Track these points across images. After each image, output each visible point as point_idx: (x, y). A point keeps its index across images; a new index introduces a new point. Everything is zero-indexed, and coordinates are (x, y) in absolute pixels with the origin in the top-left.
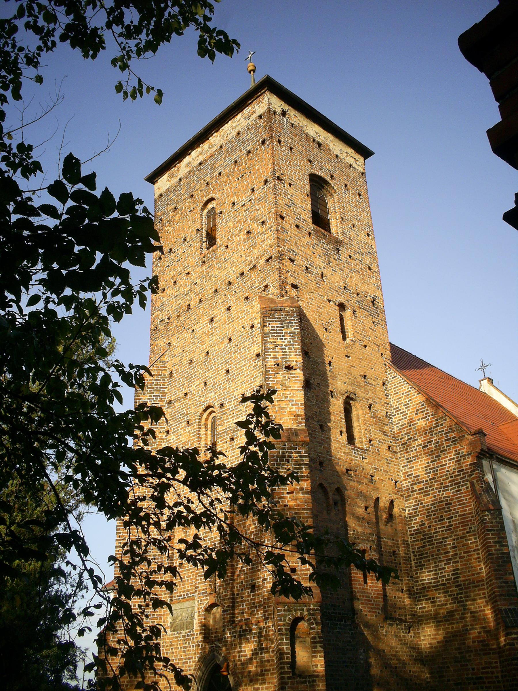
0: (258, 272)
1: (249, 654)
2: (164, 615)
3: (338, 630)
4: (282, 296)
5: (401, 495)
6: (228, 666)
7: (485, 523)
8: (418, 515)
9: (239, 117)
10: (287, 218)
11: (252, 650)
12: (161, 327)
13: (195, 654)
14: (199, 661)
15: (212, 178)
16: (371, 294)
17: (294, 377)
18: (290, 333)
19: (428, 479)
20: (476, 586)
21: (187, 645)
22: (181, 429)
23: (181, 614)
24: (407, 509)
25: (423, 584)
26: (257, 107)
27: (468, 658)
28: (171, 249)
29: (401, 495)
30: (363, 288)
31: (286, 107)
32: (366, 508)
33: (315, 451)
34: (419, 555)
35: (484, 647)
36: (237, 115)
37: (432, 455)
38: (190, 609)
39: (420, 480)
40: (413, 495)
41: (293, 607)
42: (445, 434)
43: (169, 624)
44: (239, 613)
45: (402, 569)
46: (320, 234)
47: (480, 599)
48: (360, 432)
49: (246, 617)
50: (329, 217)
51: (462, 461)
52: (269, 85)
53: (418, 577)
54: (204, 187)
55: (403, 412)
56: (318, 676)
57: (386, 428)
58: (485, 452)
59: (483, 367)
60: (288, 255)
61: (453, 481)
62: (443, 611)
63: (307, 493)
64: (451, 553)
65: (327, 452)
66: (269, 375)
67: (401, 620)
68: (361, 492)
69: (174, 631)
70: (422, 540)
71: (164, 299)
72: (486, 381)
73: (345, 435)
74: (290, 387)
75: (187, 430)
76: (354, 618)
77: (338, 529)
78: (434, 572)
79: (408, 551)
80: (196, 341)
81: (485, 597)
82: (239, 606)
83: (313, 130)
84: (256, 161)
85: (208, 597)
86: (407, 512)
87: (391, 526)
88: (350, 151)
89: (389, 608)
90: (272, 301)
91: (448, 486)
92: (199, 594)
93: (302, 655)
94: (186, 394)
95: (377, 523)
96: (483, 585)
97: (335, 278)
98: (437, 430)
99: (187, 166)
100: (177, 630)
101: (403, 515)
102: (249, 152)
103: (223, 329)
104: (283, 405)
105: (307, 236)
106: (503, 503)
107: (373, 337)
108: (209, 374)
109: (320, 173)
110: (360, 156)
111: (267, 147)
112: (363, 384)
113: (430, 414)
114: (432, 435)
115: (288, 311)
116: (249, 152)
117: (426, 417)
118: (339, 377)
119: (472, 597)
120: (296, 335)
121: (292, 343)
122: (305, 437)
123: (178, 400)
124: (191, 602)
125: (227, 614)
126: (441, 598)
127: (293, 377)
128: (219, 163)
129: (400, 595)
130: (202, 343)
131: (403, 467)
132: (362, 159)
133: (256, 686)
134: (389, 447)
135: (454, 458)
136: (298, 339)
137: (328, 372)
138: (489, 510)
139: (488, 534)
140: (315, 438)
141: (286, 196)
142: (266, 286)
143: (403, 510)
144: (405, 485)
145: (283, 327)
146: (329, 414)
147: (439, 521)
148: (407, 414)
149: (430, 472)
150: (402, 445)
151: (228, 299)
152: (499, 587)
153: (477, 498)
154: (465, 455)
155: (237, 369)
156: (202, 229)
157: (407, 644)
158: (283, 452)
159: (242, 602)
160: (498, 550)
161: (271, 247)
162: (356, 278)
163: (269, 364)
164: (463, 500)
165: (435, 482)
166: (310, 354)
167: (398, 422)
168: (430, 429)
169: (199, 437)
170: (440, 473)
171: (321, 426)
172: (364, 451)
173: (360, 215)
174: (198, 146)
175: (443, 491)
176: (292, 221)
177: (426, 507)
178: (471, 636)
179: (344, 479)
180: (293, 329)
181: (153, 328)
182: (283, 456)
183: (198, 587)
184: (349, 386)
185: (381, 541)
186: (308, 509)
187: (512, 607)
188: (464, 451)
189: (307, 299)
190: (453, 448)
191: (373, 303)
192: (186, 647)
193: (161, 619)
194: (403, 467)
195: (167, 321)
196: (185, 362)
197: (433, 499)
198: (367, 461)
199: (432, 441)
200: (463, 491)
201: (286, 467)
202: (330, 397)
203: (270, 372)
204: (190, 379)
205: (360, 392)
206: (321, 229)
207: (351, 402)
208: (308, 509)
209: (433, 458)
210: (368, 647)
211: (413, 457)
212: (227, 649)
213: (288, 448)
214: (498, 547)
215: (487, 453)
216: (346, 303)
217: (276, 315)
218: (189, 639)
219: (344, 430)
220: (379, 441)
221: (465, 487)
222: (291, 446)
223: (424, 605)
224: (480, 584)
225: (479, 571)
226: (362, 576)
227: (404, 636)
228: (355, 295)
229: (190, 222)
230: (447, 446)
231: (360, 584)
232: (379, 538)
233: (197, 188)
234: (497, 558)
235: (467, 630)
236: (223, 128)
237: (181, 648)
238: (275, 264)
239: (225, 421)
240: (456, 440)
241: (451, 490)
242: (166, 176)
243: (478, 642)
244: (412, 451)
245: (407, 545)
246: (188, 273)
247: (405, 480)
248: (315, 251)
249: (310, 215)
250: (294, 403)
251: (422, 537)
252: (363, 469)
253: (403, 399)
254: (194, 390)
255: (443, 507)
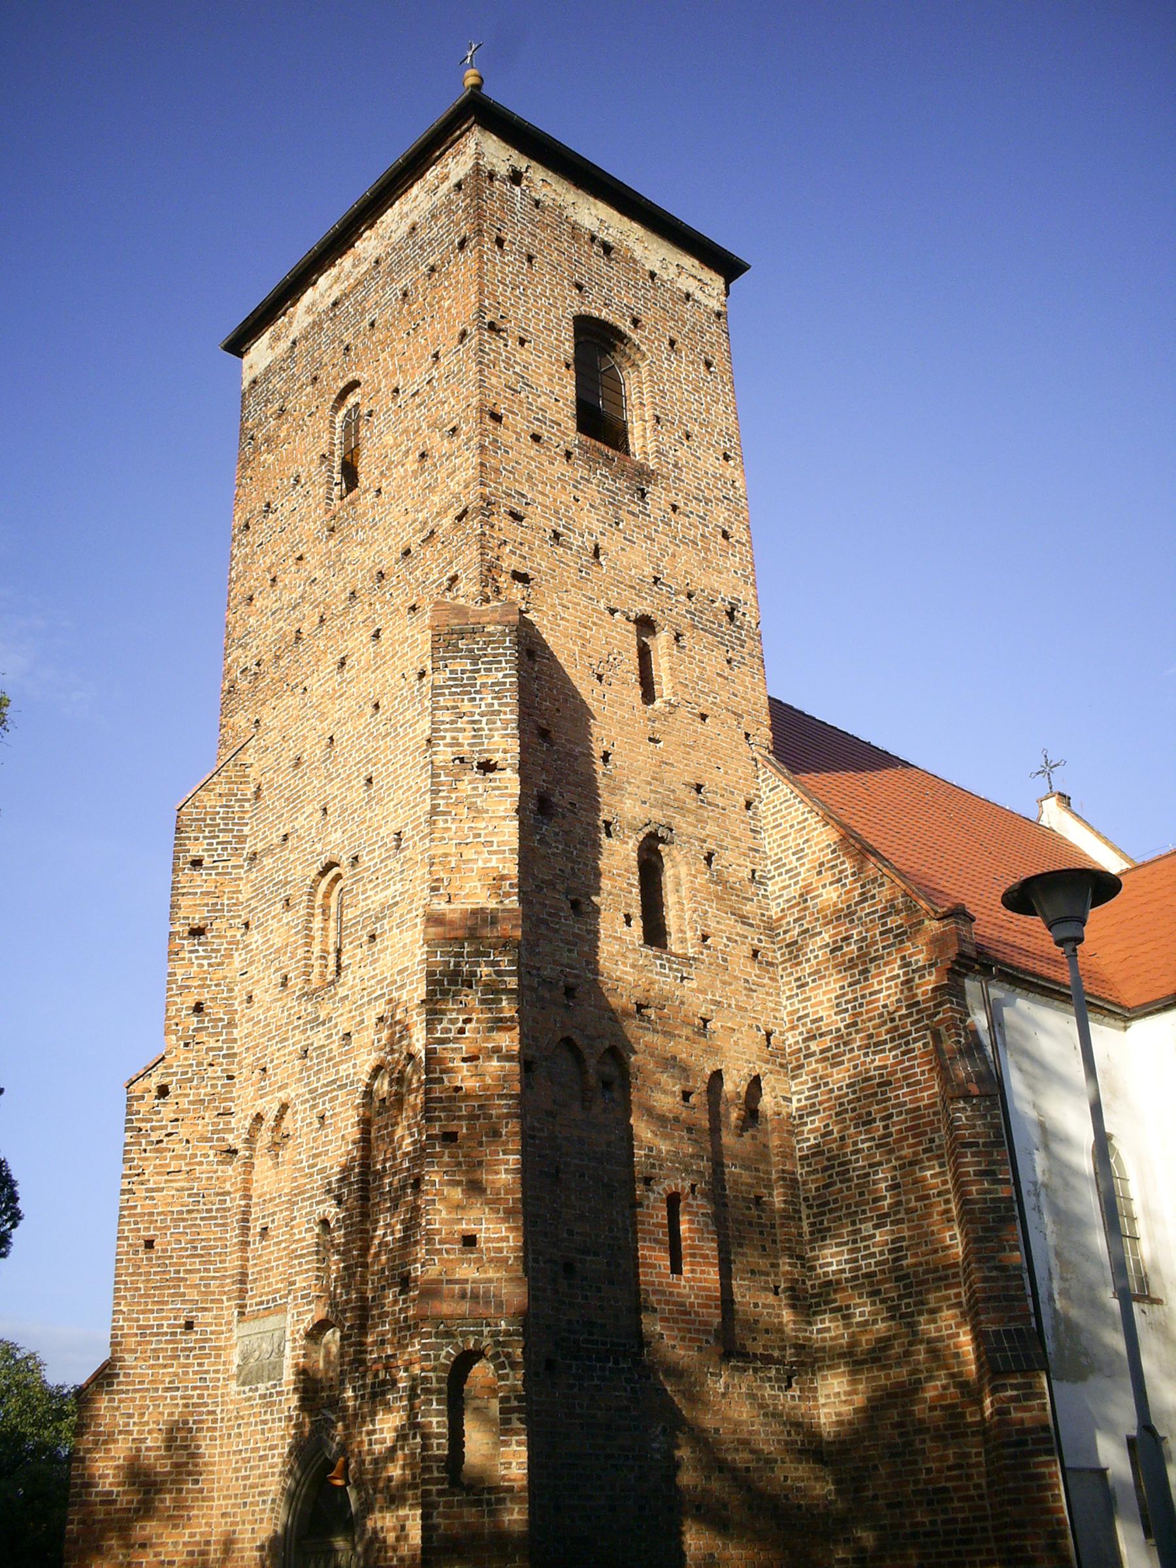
0: (440, 546)
1: (389, 1436)
2: (225, 1348)
3: (596, 1382)
4: (487, 600)
5: (781, 1065)
6: (346, 1465)
7: (958, 1128)
8: (818, 1112)
9: (415, 190)
10: (508, 419)
11: (396, 1429)
12: (243, 685)
13: (283, 1437)
14: (290, 1453)
15: (356, 336)
16: (726, 593)
17: (498, 788)
18: (493, 684)
19: (841, 1025)
20: (940, 1279)
21: (268, 1417)
22: (274, 917)
23: (259, 1346)
24: (795, 1098)
25: (826, 1274)
26: (452, 165)
27: (918, 1446)
28: (268, 505)
29: (781, 1065)
30: (702, 581)
31: (522, 163)
32: (686, 1095)
33: (555, 962)
34: (818, 1206)
35: (953, 1425)
36: (411, 186)
37: (850, 968)
38: (277, 1334)
39: (824, 1029)
40: (809, 1064)
41: (459, 1326)
42: (881, 917)
43: (234, 1369)
44: (374, 1343)
45: (779, 1238)
46: (595, 456)
47: (949, 1307)
48: (681, 918)
49: (389, 1352)
50: (627, 416)
51: (917, 981)
52: (480, 111)
53: (817, 1258)
54: (339, 358)
55: (790, 870)
56: (510, 1489)
57: (748, 908)
58: (970, 958)
59: (1048, 768)
60: (505, 504)
61: (896, 1028)
62: (868, 1337)
63: (509, 1058)
64: (888, 1201)
65: (588, 963)
66: (440, 784)
67: (768, 1360)
68: (674, 1058)
69: (243, 1384)
70: (825, 1169)
71: (252, 620)
72: (1053, 801)
73: (637, 924)
74: (487, 811)
75: (285, 921)
76: (640, 1354)
77: (609, 1144)
78: (850, 1246)
79: (793, 1195)
80: (311, 713)
81: (959, 1305)
82: (375, 1326)
83: (593, 214)
84: (446, 288)
85: (313, 1306)
86: (795, 1104)
87: (754, 1137)
88: (689, 262)
89: (737, 1330)
90: (461, 611)
91: (885, 1042)
92: (295, 1298)
93: (477, 1442)
94: (285, 838)
95: (715, 1131)
96: (956, 1275)
97: (631, 557)
98: (863, 909)
99: (309, 311)
100: (250, 1383)
101: (784, 1111)
102: (433, 269)
103: (364, 683)
104: (469, 854)
105: (560, 460)
106: (1015, 1082)
107: (724, 695)
108: (332, 789)
109: (604, 314)
110: (713, 275)
111: (470, 254)
112: (692, 805)
113: (849, 872)
114: (852, 921)
115: (490, 634)
116: (433, 269)
117: (839, 880)
118: (629, 789)
119: (932, 1305)
120: (508, 690)
121: (496, 707)
122: (514, 926)
123: (269, 851)
124: (279, 1317)
125: (350, 1346)
126: (862, 1310)
127: (494, 789)
128: (373, 297)
129: (771, 1299)
130: (322, 716)
131: (788, 998)
132: (719, 282)
133: (401, 1513)
134: (755, 953)
135: (898, 976)
136: (511, 698)
137: (599, 776)
138: (967, 1097)
139: (964, 1155)
140: (556, 931)
141: (509, 365)
142: (454, 579)
143: (785, 1099)
144: (791, 1041)
145: (478, 671)
146: (598, 874)
147: (864, 1124)
148: (799, 874)
149: (846, 1010)
150: (788, 946)
151: (376, 612)
152: (985, 1279)
153: (943, 1070)
154: (924, 967)
155: (389, 775)
156: (332, 453)
157: (781, 1415)
158: (457, 964)
159: (381, 1316)
160: (986, 1192)
161: (466, 487)
162: (686, 558)
163: (441, 758)
164: (915, 1074)
165: (857, 1032)
166: (553, 734)
167: (779, 894)
168: (849, 907)
169: (307, 936)
170: (867, 1012)
171: (575, 905)
172: (687, 960)
173: (708, 410)
174: (333, 264)
175: (874, 1053)
176: (522, 425)
177: (837, 1093)
178: (927, 1395)
179: (632, 1028)
180: (500, 675)
181: (226, 688)
182: (457, 973)
183: (294, 1283)
184: (654, 811)
185: (723, 1173)
186: (512, 1097)
187: (1012, 1326)
188: (921, 959)
189: (553, 606)
190: (898, 950)
191: (730, 615)
192: (265, 1422)
193: (218, 1356)
194: (788, 998)
195: (255, 669)
196: (286, 764)
197: (852, 1072)
198: (694, 985)
199: (851, 936)
200: (916, 1053)
201: (462, 998)
202: (603, 836)
203: (443, 778)
204: (294, 801)
205: (682, 824)
206: (598, 444)
207: (661, 846)
208: (512, 1097)
209: (852, 976)
210: (675, 1423)
211: (809, 975)
212: (346, 1427)
213: (469, 955)
214: (986, 1185)
215: (976, 961)
216: (657, 616)
217: (462, 644)
218: (273, 1404)
219: (636, 912)
220: (729, 939)
221: (920, 1044)
222: (477, 950)
223: (827, 1324)
224: (950, 1272)
225: (948, 1242)
226: (667, 1255)
227: (776, 1397)
228: (682, 598)
229: (310, 439)
230: (884, 948)
231: (659, 1275)
232: (718, 1165)
233: (326, 359)
234: (982, 1211)
235: (919, 1381)
236: (383, 218)
237: (256, 1425)
238: (474, 525)
239: (361, 897)
240: (905, 932)
241: (890, 1050)
242: (265, 338)
243: (943, 1408)
244: (808, 960)
245: (792, 1183)
246: (300, 558)
247: (793, 1028)
248: (579, 495)
249: (571, 410)
250: (495, 848)
251: (826, 1163)
252: (682, 1003)
253: (791, 836)
254: (303, 827)
255: (870, 1093)
